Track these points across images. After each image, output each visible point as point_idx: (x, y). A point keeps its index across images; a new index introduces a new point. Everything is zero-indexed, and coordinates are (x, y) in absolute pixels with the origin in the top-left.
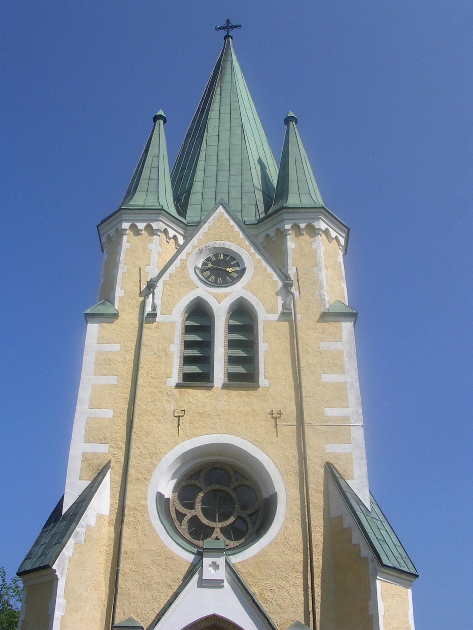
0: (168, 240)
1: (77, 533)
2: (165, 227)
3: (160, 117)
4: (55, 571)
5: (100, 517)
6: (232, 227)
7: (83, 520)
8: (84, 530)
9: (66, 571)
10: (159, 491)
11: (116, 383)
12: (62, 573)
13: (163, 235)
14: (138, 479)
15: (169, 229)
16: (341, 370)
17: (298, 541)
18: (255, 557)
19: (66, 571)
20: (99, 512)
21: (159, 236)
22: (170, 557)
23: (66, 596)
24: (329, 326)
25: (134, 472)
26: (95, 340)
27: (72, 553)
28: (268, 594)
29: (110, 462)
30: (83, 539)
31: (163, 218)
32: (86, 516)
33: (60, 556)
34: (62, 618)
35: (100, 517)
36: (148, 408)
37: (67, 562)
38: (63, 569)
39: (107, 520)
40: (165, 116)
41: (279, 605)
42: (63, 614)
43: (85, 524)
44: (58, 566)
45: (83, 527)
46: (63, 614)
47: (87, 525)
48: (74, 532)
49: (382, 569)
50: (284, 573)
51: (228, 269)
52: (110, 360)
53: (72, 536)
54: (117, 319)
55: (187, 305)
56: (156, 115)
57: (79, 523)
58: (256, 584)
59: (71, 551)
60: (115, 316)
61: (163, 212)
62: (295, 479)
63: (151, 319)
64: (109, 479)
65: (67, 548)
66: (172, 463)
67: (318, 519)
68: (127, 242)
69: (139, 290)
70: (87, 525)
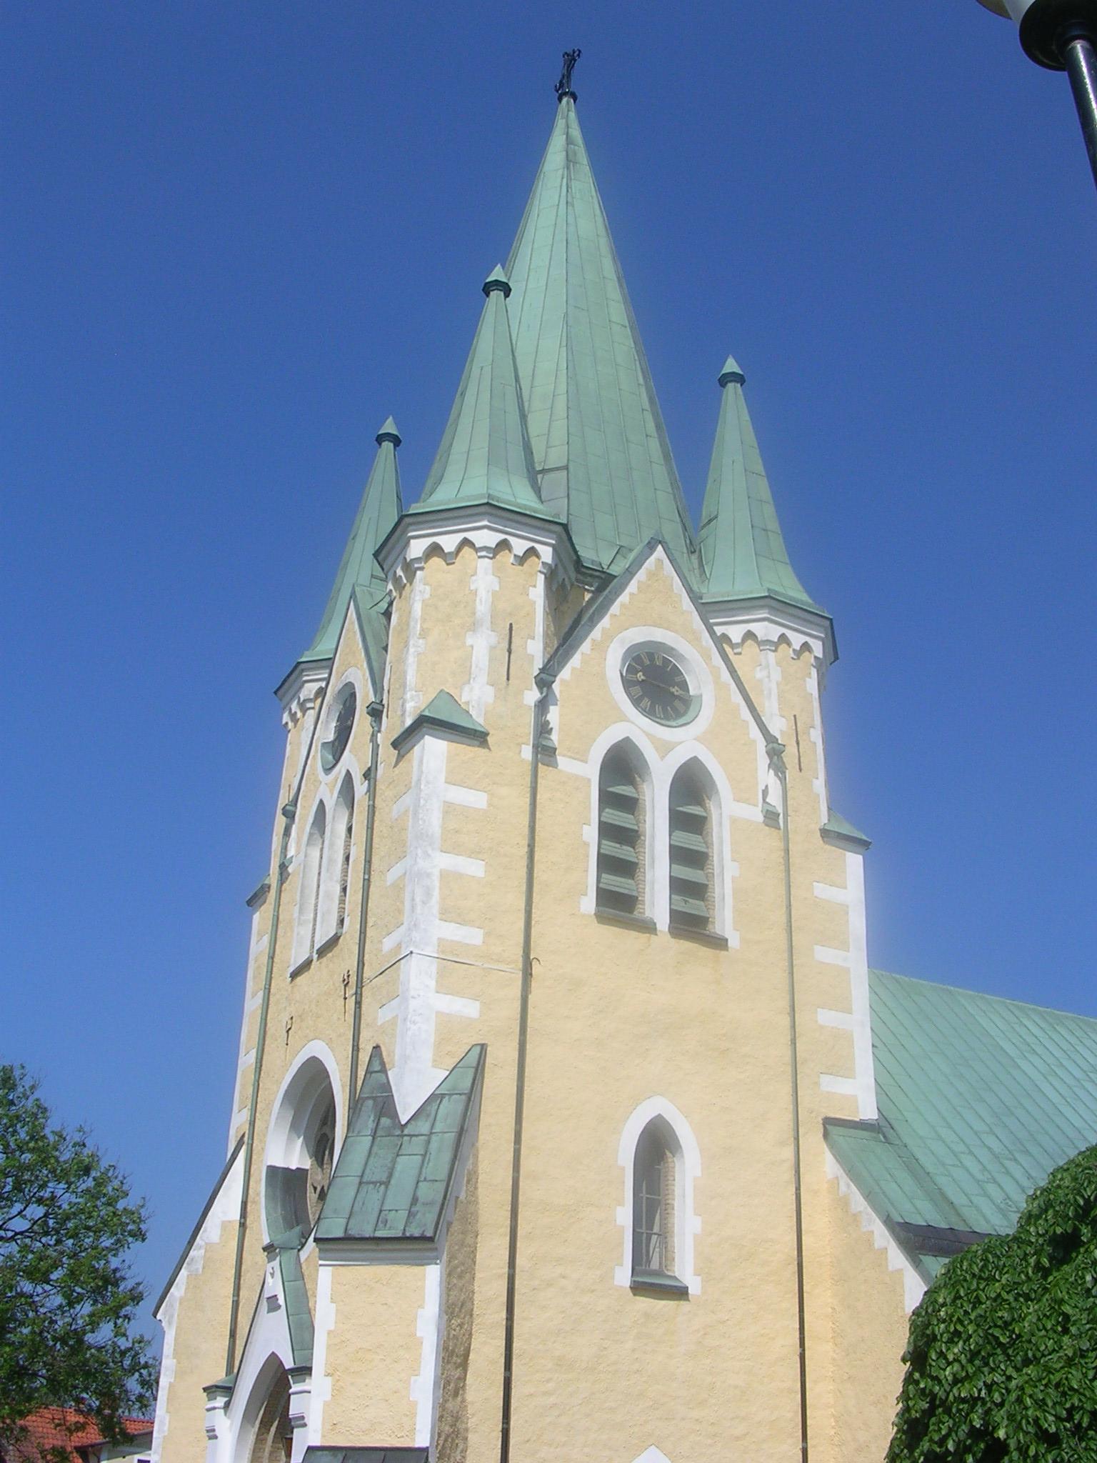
1: (192, 1260)
3: (389, 437)
5: (225, 1225)
7: (201, 1238)
8: (203, 1251)
10: (269, 1164)
12: (170, 1323)
16: (844, 946)
23: (176, 1354)
24: (832, 851)
27: (183, 1291)
35: (225, 1225)
38: (172, 1316)
42: (172, 1380)
43: (203, 1243)
44: (164, 1314)
45: (200, 1248)
46: (172, 1380)
47: (206, 1243)
48: (187, 1259)
53: (185, 1265)
56: (379, 435)
57: (195, 1244)
59: (183, 1288)
61: (303, 666)
65: (177, 1285)
67: (647, 1050)
70: (206, 1243)
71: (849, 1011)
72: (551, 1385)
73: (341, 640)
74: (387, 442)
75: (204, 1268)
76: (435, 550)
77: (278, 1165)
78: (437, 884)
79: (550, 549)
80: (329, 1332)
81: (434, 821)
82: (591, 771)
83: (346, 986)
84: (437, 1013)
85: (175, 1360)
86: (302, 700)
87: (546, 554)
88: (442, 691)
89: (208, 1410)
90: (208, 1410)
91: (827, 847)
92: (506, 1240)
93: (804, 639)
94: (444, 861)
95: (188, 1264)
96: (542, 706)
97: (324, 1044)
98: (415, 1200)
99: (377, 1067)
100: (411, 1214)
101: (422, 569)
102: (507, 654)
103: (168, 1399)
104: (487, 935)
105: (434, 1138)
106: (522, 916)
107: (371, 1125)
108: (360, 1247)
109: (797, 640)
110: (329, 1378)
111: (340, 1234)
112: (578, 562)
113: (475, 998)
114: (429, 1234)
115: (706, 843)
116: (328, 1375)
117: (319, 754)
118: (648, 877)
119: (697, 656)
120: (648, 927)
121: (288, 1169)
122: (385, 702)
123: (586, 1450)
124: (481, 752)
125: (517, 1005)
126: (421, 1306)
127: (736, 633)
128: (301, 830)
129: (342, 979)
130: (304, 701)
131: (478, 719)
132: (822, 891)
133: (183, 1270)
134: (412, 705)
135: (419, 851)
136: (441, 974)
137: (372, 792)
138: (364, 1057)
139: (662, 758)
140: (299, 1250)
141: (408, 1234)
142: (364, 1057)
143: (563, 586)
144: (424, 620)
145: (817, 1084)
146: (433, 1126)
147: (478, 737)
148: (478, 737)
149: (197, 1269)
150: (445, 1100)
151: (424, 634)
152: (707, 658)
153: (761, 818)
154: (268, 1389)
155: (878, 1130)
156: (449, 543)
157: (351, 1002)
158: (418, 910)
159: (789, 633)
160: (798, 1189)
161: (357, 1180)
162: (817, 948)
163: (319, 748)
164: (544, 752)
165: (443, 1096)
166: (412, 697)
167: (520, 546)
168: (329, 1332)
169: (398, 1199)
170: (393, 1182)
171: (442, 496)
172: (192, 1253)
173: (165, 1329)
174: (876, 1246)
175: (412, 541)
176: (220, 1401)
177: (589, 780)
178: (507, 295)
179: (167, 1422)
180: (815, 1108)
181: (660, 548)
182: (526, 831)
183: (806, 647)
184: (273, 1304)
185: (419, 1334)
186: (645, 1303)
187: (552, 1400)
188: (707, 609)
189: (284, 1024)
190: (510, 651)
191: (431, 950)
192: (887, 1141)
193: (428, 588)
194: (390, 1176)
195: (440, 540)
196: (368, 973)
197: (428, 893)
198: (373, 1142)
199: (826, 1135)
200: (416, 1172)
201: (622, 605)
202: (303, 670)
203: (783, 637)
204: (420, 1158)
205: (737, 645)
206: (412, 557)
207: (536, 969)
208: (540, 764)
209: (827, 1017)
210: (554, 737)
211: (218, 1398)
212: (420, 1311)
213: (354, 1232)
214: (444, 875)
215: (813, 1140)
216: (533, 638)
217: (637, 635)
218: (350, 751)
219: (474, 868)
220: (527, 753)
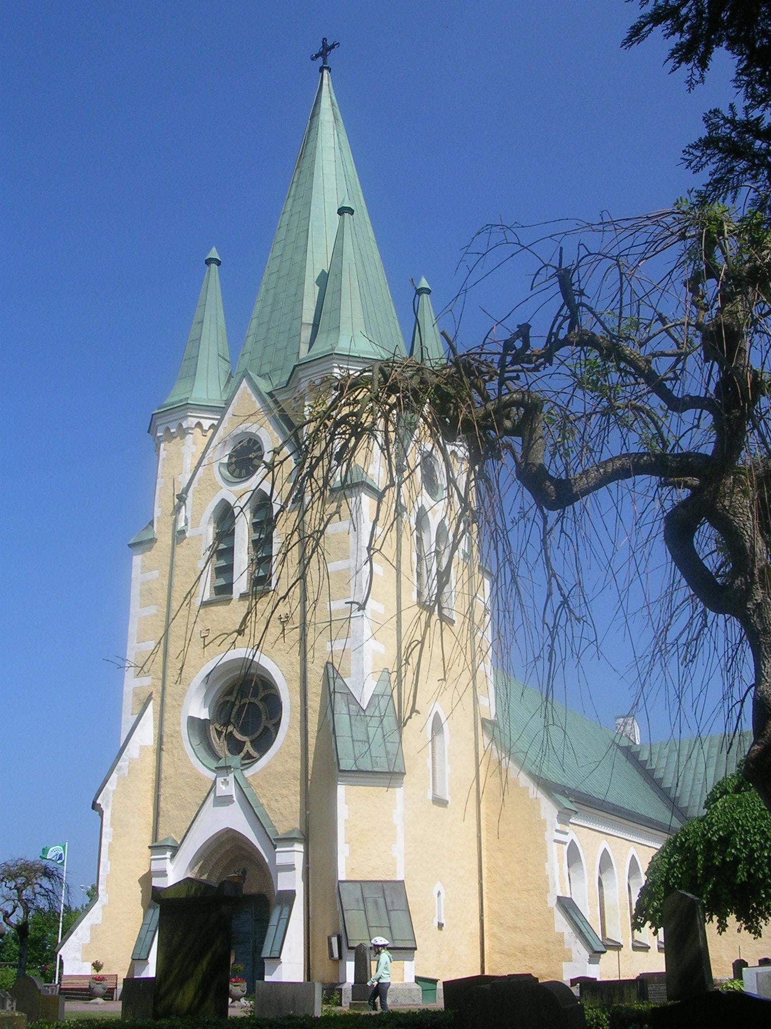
0: (204, 434)
2: (196, 420)
4: (100, 805)
5: (143, 748)
6: (254, 402)
8: (127, 763)
9: (111, 803)
10: (190, 715)
11: (156, 612)
12: (107, 806)
13: (198, 430)
14: (174, 707)
15: (202, 421)
17: (297, 750)
18: (263, 769)
19: (111, 803)
20: (141, 744)
21: (192, 434)
22: (199, 778)
23: (112, 824)
25: (170, 700)
26: (139, 571)
28: (274, 804)
29: (151, 694)
30: (126, 772)
31: (191, 412)
32: (129, 750)
33: (103, 791)
34: (110, 844)
36: (181, 633)
37: (111, 795)
38: (108, 802)
39: (151, 749)
40: (220, 260)
41: (281, 814)
44: (102, 800)
46: (111, 841)
47: (130, 758)
48: (116, 768)
49: (341, 774)
50: (286, 782)
51: (251, 456)
52: (150, 589)
53: (115, 771)
54: (156, 542)
55: (214, 512)
57: (122, 758)
58: (264, 795)
59: (115, 784)
60: (153, 541)
61: (189, 406)
62: (297, 685)
63: (182, 537)
64: (152, 710)
66: (200, 685)
68: (164, 450)
69: (172, 505)
70: (130, 758)
74: (214, 264)
75: (129, 773)
77: (195, 716)
85: (112, 829)
95: (117, 770)
103: (109, 852)
108: (350, 775)
110: (347, 845)
121: (200, 719)
133: (114, 774)
149: (124, 774)
155: (492, 723)
172: (120, 764)
173: (104, 809)
178: (352, 214)
179: (109, 866)
202: (188, 408)
211: (168, 853)
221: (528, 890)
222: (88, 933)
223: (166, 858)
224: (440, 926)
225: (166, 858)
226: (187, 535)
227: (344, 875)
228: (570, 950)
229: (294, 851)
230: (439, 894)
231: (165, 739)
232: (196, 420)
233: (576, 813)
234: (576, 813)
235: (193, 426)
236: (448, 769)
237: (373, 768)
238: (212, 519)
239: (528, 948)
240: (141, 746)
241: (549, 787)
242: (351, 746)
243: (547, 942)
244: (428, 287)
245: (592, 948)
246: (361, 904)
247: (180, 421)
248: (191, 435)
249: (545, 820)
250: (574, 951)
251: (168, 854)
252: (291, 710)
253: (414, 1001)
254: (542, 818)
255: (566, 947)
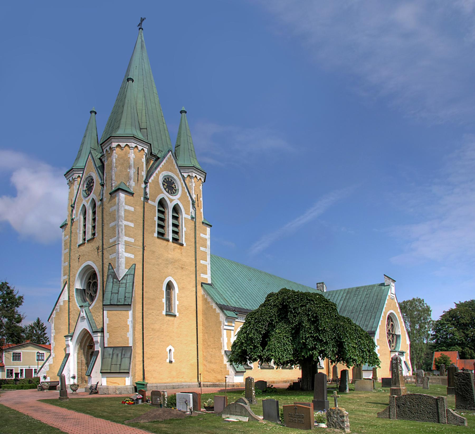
5: (64, 301)
8: (59, 307)
10: (76, 288)
30: (59, 310)
37: (54, 319)
38: (52, 321)
59: (55, 315)
71: (206, 261)
72: (151, 334)
73: (87, 164)
76: (119, 146)
78: (124, 228)
79: (147, 149)
80: (107, 324)
81: (122, 213)
82: (156, 204)
83: (98, 249)
84: (125, 257)
86: (74, 178)
87: (146, 150)
88: (122, 182)
89: (66, 341)
90: (66, 341)
91: (203, 226)
92: (141, 305)
93: (200, 177)
94: (125, 223)
96: (145, 188)
97: (92, 262)
98: (125, 297)
99: (111, 268)
100: (125, 300)
101: (115, 150)
102: (137, 175)
104: (135, 240)
105: (127, 284)
106: (142, 236)
107: (112, 281)
109: (199, 177)
110: (108, 334)
111: (109, 304)
112: (151, 153)
113: (133, 254)
114: (130, 304)
115: (179, 223)
116: (108, 333)
117: (82, 193)
118: (167, 229)
119: (178, 180)
120: (168, 240)
122: (105, 182)
123: (158, 346)
124: (132, 197)
125: (142, 256)
126: (128, 319)
127: (185, 175)
128: (77, 211)
129: (96, 247)
130: (75, 178)
131: (132, 190)
132: (202, 235)
134: (115, 185)
135: (120, 220)
136: (125, 248)
137: (102, 205)
138: (106, 266)
139: (171, 203)
140: (89, 307)
141: (125, 304)
142: (106, 266)
143: (148, 159)
144: (116, 163)
145: (200, 275)
146: (127, 281)
147: (132, 194)
148: (132, 194)
150: (129, 276)
151: (116, 167)
152: (180, 180)
153: (190, 218)
154: (82, 336)
156: (123, 145)
157: (100, 253)
158: (120, 234)
159: (197, 176)
160: (196, 296)
161: (111, 292)
162: (201, 247)
163: (82, 191)
164: (146, 199)
165: (128, 275)
166: (114, 182)
167: (140, 148)
168: (107, 324)
169: (121, 296)
170: (119, 293)
171: (120, 132)
172: (56, 308)
174: (213, 308)
175: (113, 143)
176: (70, 339)
177: (155, 206)
179: (54, 343)
180: (199, 281)
181: (170, 152)
182: (142, 217)
183: (200, 179)
184: (83, 318)
185: (128, 324)
186: (169, 318)
187: (151, 337)
188: (180, 167)
189: (77, 257)
190: (138, 174)
191: (123, 243)
192: (213, 288)
193: (117, 155)
194: (118, 292)
195: (120, 144)
196: (105, 247)
197: (122, 230)
198: (113, 284)
199: (202, 286)
200: (124, 291)
201: (162, 165)
202: (74, 171)
203: (196, 176)
204: (125, 288)
205: (186, 178)
206: (113, 147)
207: (145, 248)
208: (145, 202)
209: (202, 262)
210: (148, 196)
212: (128, 320)
213: (112, 303)
214: (125, 226)
215: (199, 287)
216: (143, 171)
217: (165, 173)
218: (93, 193)
219: (132, 225)
220: (142, 199)
221: (215, 348)
222: (48, 367)
223: (68, 340)
224: (171, 362)
225: (68, 340)
226: (75, 220)
227: (107, 345)
228: (228, 371)
229: (98, 336)
230: (170, 350)
231: (70, 298)
232: (78, 175)
233: (237, 318)
234: (237, 318)
235: (77, 178)
236: (177, 303)
237: (117, 303)
238: (81, 213)
239: (215, 370)
240: (64, 301)
241: (222, 308)
242: (110, 295)
243: (221, 368)
244: (185, 110)
245: (236, 371)
246: (111, 356)
247: (72, 176)
248: (77, 181)
249: (221, 321)
250: (230, 372)
251: (70, 339)
252: (100, 283)
253: (128, 392)
254: (220, 320)
255: (227, 370)
